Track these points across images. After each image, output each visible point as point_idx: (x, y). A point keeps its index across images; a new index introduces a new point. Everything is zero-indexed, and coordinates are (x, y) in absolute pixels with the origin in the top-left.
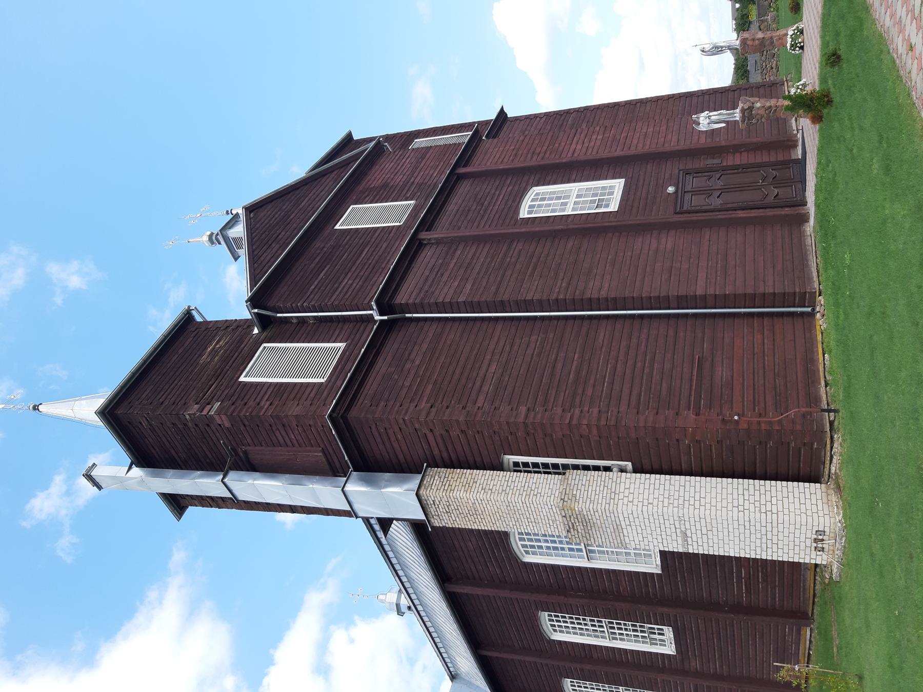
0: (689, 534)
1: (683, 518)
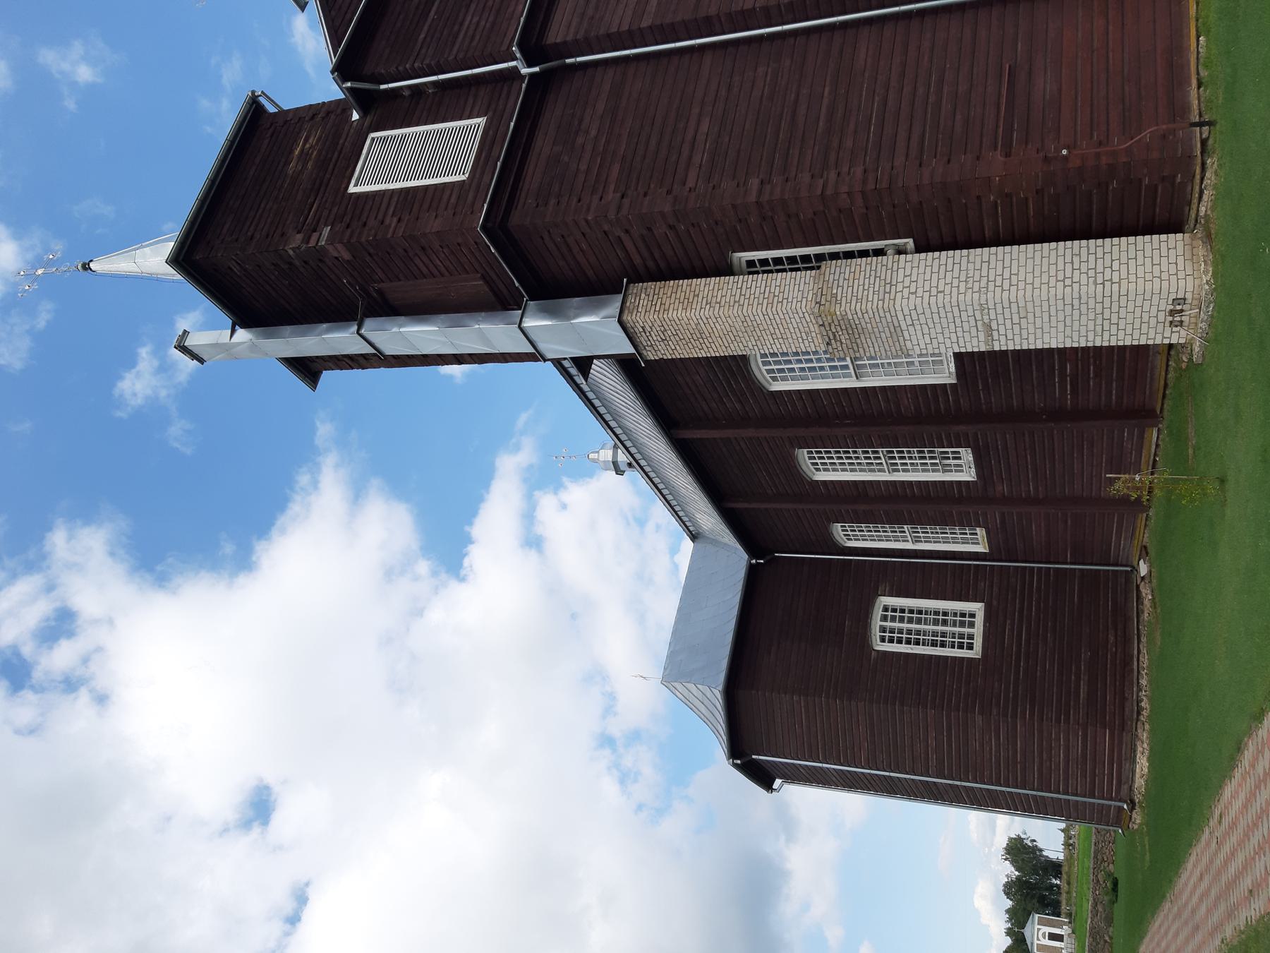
0: (994, 326)
1: (986, 306)
